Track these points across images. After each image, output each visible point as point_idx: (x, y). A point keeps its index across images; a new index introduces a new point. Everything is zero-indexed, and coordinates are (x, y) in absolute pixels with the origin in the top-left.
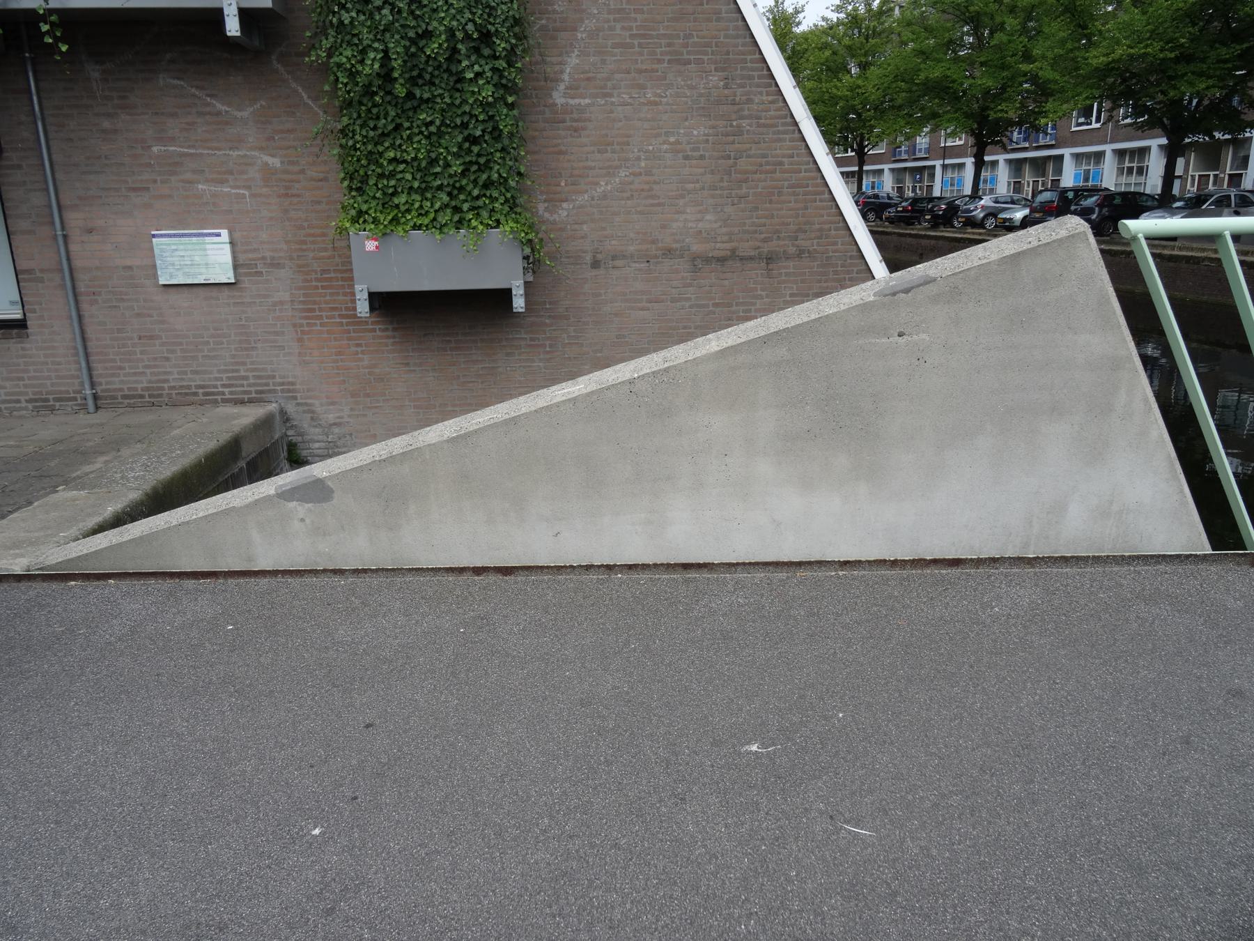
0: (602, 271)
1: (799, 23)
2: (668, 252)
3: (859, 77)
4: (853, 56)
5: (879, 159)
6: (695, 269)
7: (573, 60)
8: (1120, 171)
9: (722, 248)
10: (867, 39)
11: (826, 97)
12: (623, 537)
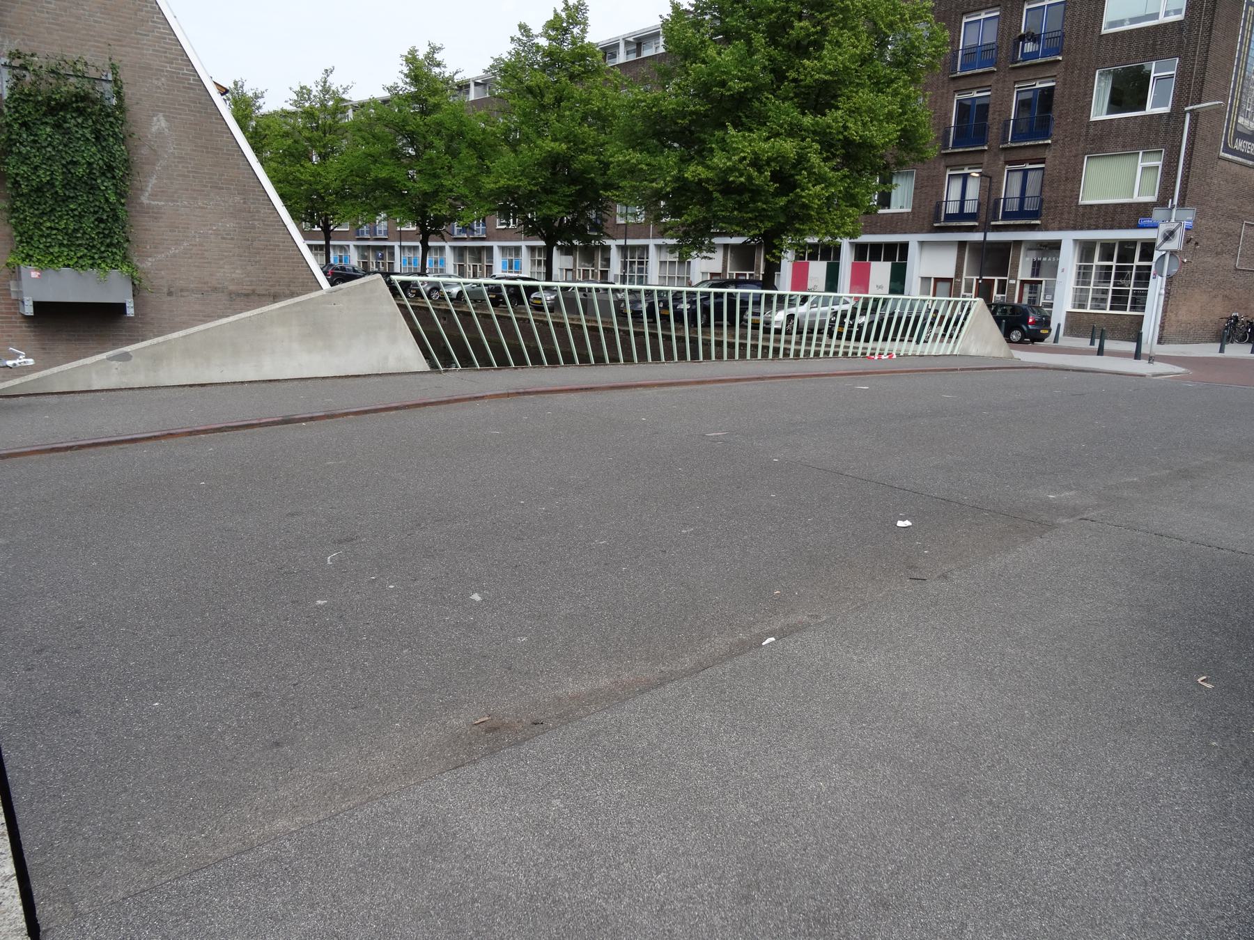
0: (174, 298)
1: (259, 107)
2: (215, 289)
3: (319, 165)
4: (314, 147)
5: (343, 236)
6: (231, 300)
7: (153, 181)
8: (533, 262)
9: (247, 288)
10: (325, 133)
11: (291, 177)
12: (247, 371)
